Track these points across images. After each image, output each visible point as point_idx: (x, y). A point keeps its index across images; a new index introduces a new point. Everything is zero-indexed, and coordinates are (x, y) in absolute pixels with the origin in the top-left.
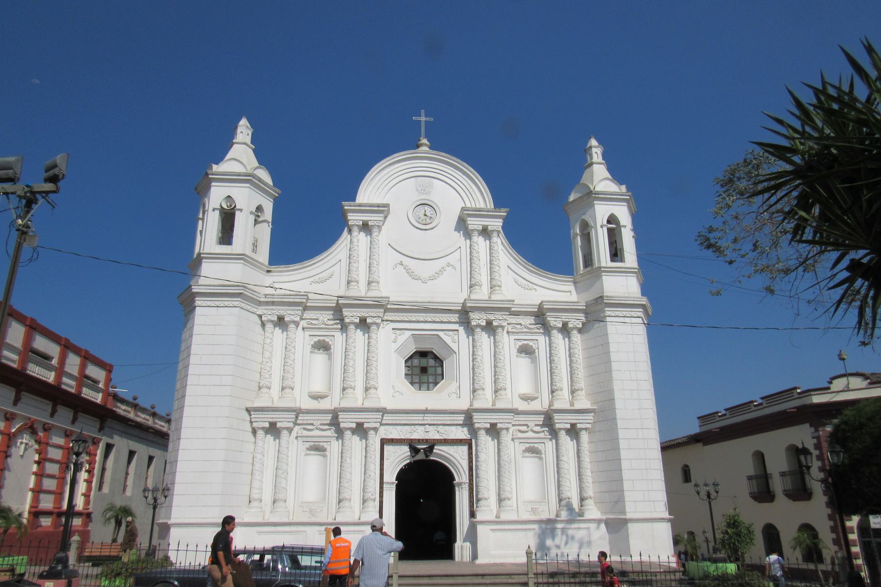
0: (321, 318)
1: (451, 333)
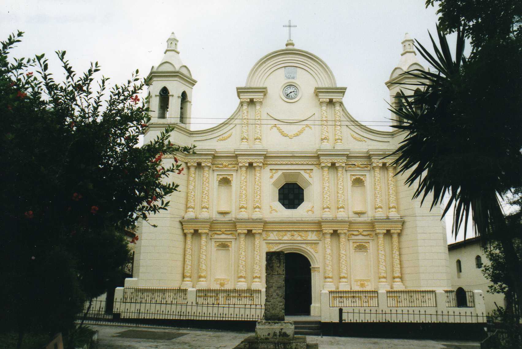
0: (224, 164)
1: (308, 171)
